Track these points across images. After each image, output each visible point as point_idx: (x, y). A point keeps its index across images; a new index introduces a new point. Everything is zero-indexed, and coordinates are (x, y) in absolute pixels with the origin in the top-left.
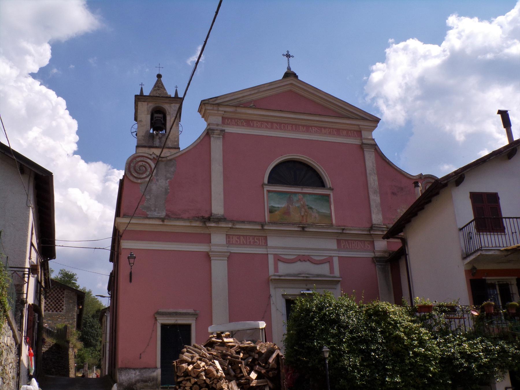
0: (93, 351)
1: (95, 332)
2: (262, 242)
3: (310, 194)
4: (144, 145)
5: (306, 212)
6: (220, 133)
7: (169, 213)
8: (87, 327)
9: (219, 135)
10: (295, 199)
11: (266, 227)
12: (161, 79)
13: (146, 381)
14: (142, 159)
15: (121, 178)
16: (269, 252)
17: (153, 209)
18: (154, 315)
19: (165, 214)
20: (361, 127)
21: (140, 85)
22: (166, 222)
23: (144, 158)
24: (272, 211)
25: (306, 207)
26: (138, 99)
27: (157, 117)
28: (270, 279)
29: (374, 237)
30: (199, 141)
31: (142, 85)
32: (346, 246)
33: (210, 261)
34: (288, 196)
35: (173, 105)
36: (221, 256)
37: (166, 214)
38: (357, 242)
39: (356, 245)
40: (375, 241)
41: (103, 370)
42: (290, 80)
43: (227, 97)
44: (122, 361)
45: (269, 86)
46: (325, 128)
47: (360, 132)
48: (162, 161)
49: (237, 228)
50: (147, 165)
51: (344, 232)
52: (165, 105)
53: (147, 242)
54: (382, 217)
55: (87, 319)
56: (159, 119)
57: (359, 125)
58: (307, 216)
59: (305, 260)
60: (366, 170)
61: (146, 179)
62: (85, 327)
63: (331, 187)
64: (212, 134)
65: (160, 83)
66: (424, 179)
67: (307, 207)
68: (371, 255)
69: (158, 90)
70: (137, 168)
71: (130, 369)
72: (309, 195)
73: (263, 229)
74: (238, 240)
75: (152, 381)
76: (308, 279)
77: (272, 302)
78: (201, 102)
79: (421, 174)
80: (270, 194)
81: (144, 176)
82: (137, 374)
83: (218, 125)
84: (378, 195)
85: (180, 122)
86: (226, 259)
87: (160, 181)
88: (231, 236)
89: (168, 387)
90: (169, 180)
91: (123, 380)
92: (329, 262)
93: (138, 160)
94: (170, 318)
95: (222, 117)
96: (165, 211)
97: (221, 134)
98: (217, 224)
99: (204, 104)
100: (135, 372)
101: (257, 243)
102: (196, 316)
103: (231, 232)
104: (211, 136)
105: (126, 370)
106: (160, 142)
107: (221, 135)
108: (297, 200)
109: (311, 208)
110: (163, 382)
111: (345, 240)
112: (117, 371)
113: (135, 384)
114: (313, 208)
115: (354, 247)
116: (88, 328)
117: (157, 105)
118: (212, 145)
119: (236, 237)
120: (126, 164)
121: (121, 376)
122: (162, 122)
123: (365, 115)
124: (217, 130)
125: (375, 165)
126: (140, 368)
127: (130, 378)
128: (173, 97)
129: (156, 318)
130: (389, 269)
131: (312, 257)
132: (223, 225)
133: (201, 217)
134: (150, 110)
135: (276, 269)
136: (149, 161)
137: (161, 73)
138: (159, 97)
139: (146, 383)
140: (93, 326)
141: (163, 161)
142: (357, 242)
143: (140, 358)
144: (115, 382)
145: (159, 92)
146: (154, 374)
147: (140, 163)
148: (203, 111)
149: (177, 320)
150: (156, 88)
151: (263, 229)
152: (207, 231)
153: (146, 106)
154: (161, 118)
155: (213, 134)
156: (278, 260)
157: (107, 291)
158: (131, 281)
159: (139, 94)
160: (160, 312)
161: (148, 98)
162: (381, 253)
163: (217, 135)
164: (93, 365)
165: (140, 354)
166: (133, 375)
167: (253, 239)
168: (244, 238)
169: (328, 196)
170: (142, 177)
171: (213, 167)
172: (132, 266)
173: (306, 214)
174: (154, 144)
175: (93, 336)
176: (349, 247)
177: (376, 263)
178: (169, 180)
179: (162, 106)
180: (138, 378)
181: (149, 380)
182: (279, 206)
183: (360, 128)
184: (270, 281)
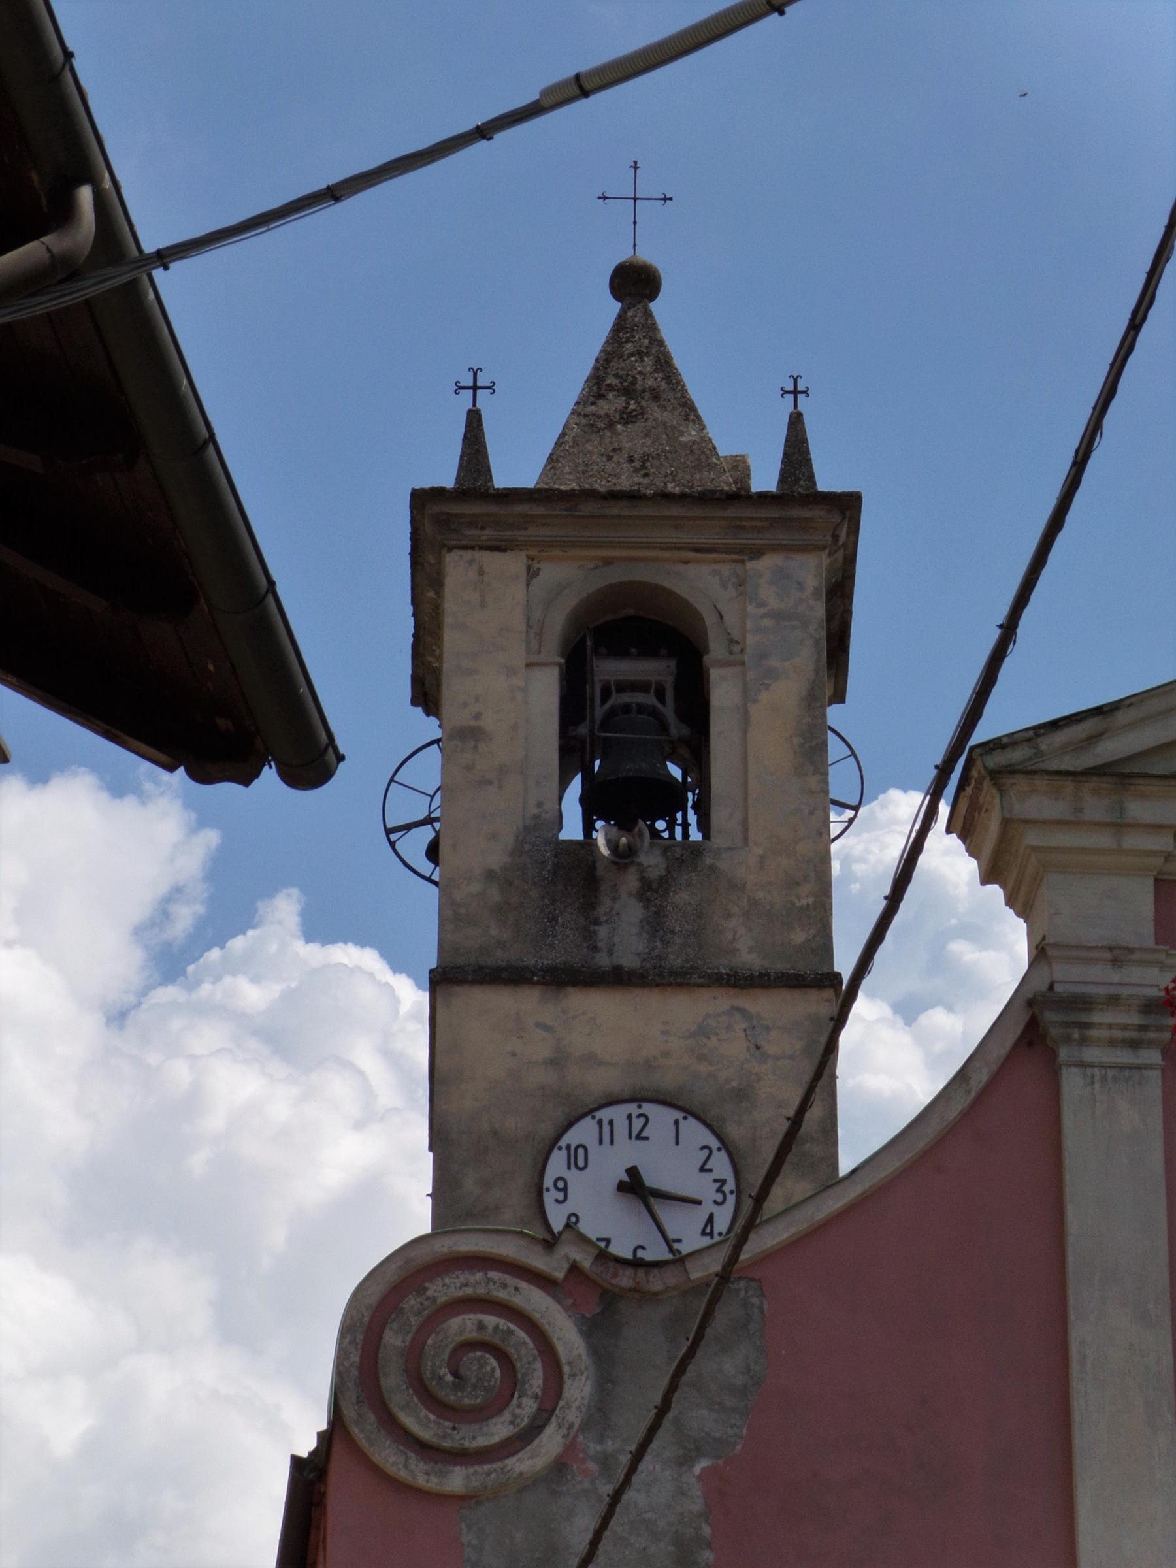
4: (500, 957)
6: (1143, 1028)
9: (1134, 1045)
12: (648, 314)
14: (475, 1282)
15: (306, 1446)
21: (459, 388)
23: (492, 1274)
26: (445, 522)
27: (622, 687)
30: (959, 1104)
31: (475, 388)
35: (766, 564)
48: (644, 1296)
50: (522, 1335)
52: (692, 570)
56: (641, 708)
61: (510, 1462)
64: (1068, 1039)
65: (639, 353)
69: (628, 418)
70: (437, 1366)
81: (499, 1430)
83: (1118, 955)
85: (839, 696)
90: (704, 1463)
93: (442, 1299)
95: (1156, 880)
97: (1151, 1035)
99: (996, 775)
104: (1064, 1053)
106: (655, 925)
107: (1150, 1044)
117: (617, 575)
118: (1070, 1142)
120: (346, 1330)
122: (664, 728)
124: (1113, 1001)
128: (764, 497)
134: (557, 622)
136: (534, 1300)
137: (646, 255)
138: (632, 497)
145: (631, 439)
147: (462, 1325)
148: (993, 827)
150: (612, 404)
153: (518, 592)
154: (660, 695)
155: (1084, 1041)
159: (447, 478)
161: (540, 510)
163: (1112, 1043)
170: (481, 1442)
174: (595, 948)
178: (704, 1463)
179: (666, 584)
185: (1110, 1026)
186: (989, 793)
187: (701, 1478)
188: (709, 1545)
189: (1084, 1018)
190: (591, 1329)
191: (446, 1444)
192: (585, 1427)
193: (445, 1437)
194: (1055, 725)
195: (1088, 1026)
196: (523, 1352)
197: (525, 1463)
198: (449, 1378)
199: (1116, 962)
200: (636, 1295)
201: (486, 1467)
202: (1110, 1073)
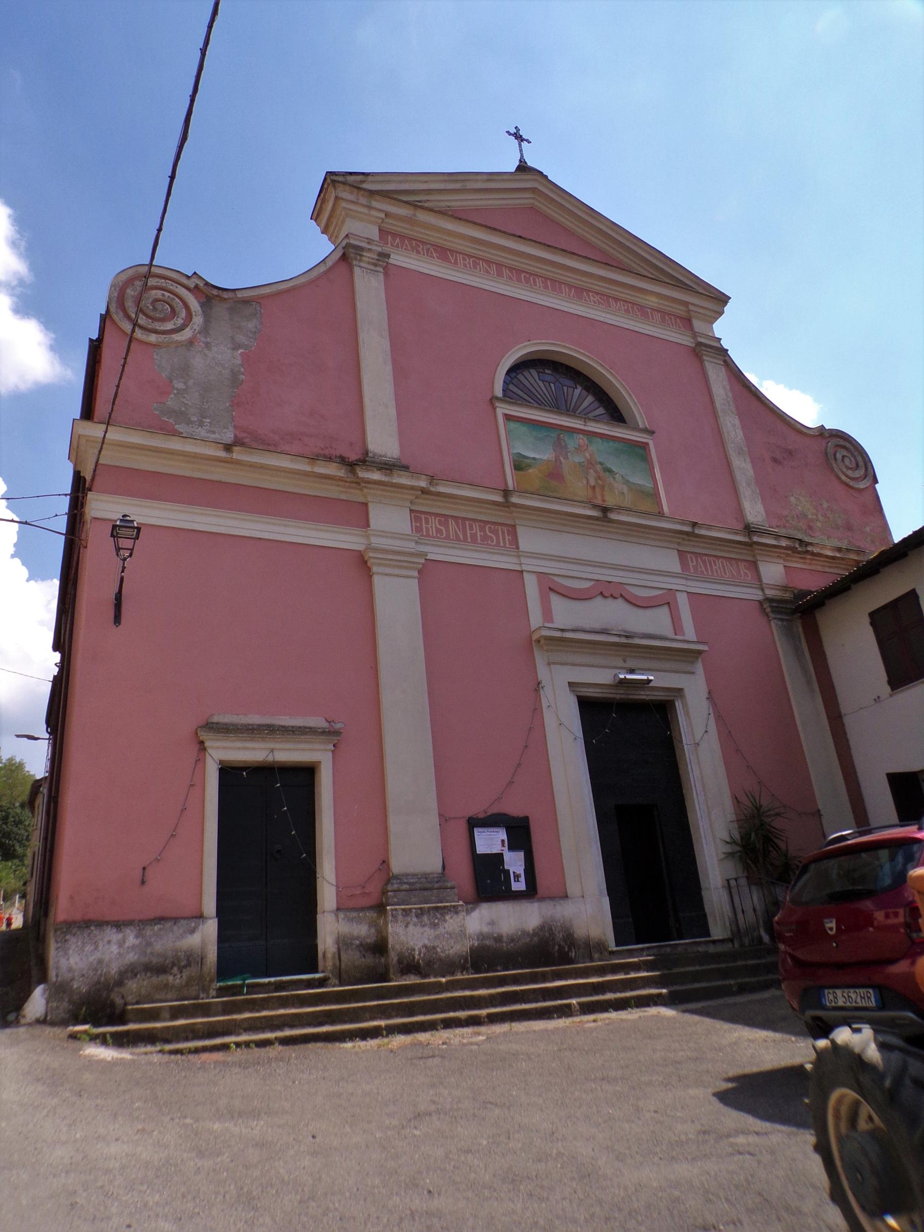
0: (18, 866)
1: (23, 832)
2: (504, 539)
3: (602, 436)
6: (378, 260)
7: (244, 435)
8: (9, 824)
9: (375, 265)
10: (572, 443)
11: (514, 499)
13: (161, 969)
14: (162, 282)
17: (194, 419)
18: (196, 729)
19: (232, 436)
20: (691, 308)
22: (238, 454)
24: (520, 465)
25: (599, 467)
28: (534, 639)
32: (699, 569)
33: (370, 576)
37: (236, 436)
39: (719, 568)
40: (759, 563)
41: (29, 904)
42: (528, 182)
43: (388, 182)
44: (72, 898)
45: (489, 180)
46: (617, 300)
47: (689, 321)
49: (439, 494)
51: (696, 532)
53: (176, 506)
54: (763, 509)
55: (9, 810)
57: (686, 304)
58: (602, 488)
62: (6, 824)
63: (648, 427)
64: (356, 259)
66: (829, 437)
68: (758, 595)
71: (101, 924)
72: (601, 438)
73: (506, 505)
75: (185, 967)
78: (325, 179)
79: (822, 426)
81: (169, 326)
82: (127, 944)
84: (748, 460)
86: (416, 574)
87: (214, 349)
89: (242, 986)
90: (241, 351)
91: (70, 970)
92: (669, 603)
94: (249, 745)
96: (231, 428)
98: (386, 475)
99: (333, 181)
100: (120, 936)
101: (493, 542)
102: (335, 739)
103: (424, 505)
105: (87, 932)
107: (380, 266)
109: (610, 471)
110: (225, 968)
111: (697, 555)
112: (52, 934)
113: (120, 983)
115: (717, 571)
116: (12, 826)
119: (437, 519)
121: (66, 954)
123: (696, 283)
125: (730, 395)
126: (140, 921)
127: (100, 961)
129: (202, 743)
130: (800, 629)
131: (627, 587)
132: (402, 479)
133: (336, 457)
135: (547, 613)
139: (162, 978)
140: (21, 822)
141: (225, 299)
142: (722, 563)
143: (143, 882)
144: (43, 978)
146: (193, 941)
147: (158, 294)
149: (272, 750)
151: (506, 505)
152: (356, 495)
155: (360, 260)
156: (550, 589)
157: (45, 726)
158: (117, 619)
160: (217, 723)
162: (778, 592)
163: (369, 263)
164: (14, 892)
165: (144, 869)
166: (114, 949)
167: (482, 529)
168: (457, 524)
169: (645, 446)
170: (162, 328)
171: (363, 336)
172: (124, 560)
173: (600, 482)
175: (20, 839)
176: (707, 570)
177: (771, 615)
178: (241, 351)
180: (132, 957)
181: (174, 964)
182: (537, 456)
184: (534, 644)
185: (369, 257)
186: (331, 189)
187: (241, 354)
188: (243, 374)
190: (202, 305)
191: (150, 327)
192: (200, 333)
193: (149, 324)
194: (351, 173)
196: (178, 305)
197: (177, 337)
198: (151, 307)
199: (368, 243)
200: (219, 299)
201: (164, 336)
202: (369, 271)
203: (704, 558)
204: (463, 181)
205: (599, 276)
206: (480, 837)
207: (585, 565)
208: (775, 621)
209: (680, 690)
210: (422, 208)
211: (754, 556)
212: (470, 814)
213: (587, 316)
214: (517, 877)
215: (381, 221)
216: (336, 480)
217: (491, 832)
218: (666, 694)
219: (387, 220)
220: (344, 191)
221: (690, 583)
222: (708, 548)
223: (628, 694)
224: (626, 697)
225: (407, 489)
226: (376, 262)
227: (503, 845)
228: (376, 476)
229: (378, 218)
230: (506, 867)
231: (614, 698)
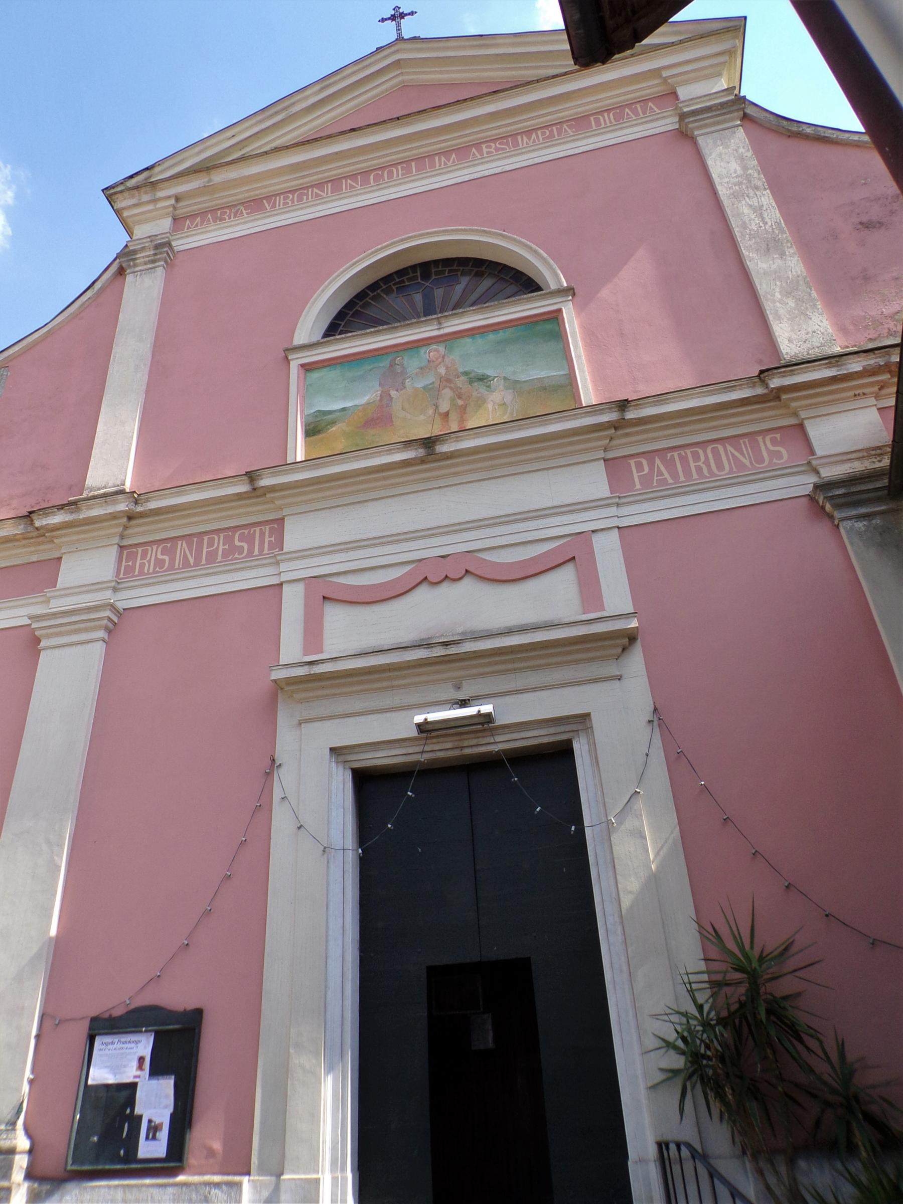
5: (460, 397)
6: (155, 254)
9: (153, 262)
10: (412, 364)
11: (265, 482)
16: (284, 578)
20: (665, 74)
29: (794, 404)
34: (385, 363)
36: (83, 626)
38: (715, 452)
40: (806, 422)
51: (630, 415)
57: (656, 73)
59: (451, 576)
60: (715, 193)
64: (129, 266)
67: (463, 378)
68: (805, 483)
74: (166, 558)
76: (452, 650)
77: (277, 794)
80: (315, 375)
86: (101, 634)
88: (688, 452)
98: (71, 513)
107: (159, 260)
108: (421, 368)
114: (488, 377)
115: (699, 469)
124: (143, 249)
131: (483, 556)
142: (715, 452)
151: (256, 493)
152: (45, 552)
155: (135, 266)
163: (145, 263)
167: (229, 540)
173: (460, 402)
176: (675, 476)
177: (837, 515)
183: (665, 80)
185: (143, 257)
189: (134, 257)
195: (135, 259)
203: (669, 455)
204: (285, 109)
205: (489, 114)
206: (101, 1052)
207: (461, 531)
208: (848, 524)
209: (584, 718)
210: (215, 167)
211: (795, 414)
212: (94, 1013)
213: (472, 178)
214: (154, 1129)
215: (171, 209)
216: (17, 540)
217: (125, 1043)
218: (552, 730)
219: (181, 204)
220: (125, 199)
221: (625, 510)
222: (681, 434)
223: (462, 748)
224: (457, 753)
225: (106, 520)
226: (153, 258)
227: (140, 1067)
228: (58, 518)
229: (168, 207)
230: (138, 1111)
231: (418, 762)
